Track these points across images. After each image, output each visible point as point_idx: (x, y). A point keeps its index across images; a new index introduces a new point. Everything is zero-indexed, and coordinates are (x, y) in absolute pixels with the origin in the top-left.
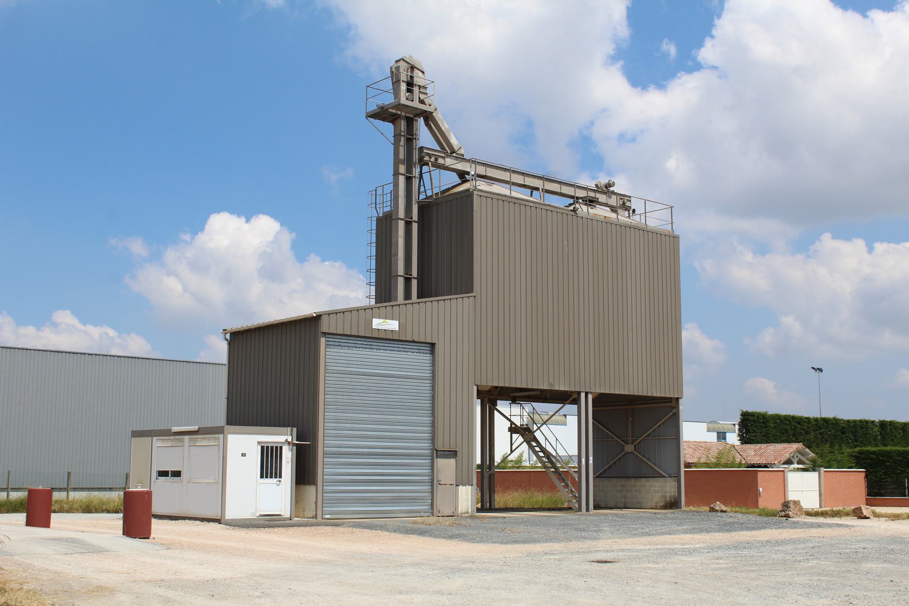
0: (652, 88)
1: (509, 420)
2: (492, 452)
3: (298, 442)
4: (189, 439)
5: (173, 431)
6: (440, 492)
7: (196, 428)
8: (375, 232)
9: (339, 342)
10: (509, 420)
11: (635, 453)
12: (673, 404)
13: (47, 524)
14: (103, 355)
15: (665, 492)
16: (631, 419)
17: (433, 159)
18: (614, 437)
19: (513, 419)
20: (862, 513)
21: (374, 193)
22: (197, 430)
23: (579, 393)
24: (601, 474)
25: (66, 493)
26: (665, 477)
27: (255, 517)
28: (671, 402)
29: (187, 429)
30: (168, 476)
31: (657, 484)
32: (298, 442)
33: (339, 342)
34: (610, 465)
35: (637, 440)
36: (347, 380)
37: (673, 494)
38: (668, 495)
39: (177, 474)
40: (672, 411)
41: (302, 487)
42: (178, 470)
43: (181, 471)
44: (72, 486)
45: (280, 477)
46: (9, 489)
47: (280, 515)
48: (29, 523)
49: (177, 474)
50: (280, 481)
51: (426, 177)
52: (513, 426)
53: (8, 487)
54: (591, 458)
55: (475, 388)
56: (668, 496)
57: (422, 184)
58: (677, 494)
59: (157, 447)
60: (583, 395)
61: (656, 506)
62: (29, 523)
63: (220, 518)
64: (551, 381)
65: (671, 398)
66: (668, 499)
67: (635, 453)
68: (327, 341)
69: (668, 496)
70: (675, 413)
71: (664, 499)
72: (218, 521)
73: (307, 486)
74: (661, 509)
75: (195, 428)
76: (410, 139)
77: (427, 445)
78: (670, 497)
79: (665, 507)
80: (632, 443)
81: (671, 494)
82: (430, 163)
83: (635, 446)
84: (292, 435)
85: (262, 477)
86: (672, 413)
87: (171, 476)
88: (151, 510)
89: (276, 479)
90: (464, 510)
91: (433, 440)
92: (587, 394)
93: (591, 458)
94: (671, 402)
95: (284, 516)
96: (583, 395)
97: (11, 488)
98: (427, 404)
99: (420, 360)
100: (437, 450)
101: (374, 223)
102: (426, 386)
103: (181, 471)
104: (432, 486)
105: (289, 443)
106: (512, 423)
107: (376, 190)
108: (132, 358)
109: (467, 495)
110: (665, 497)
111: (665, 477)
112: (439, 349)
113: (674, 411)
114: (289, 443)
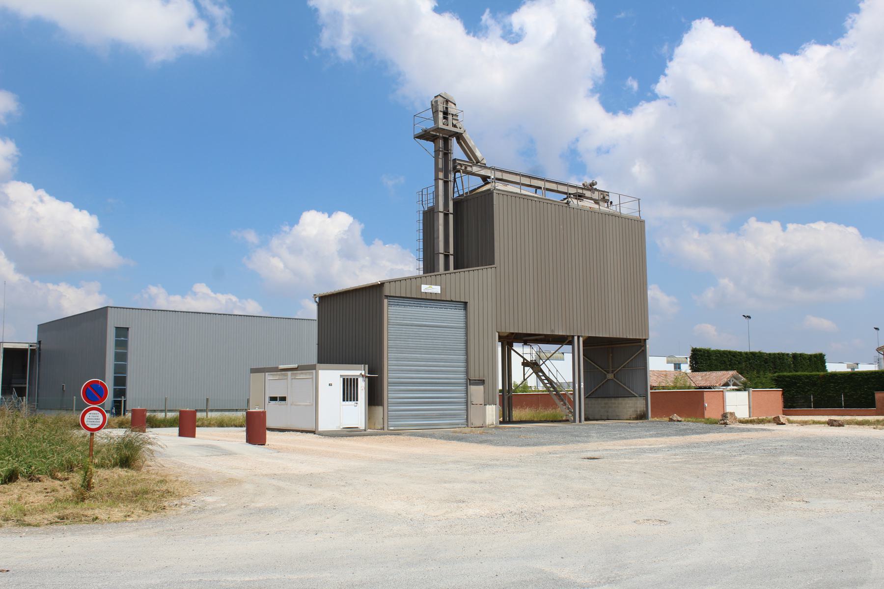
1: (522, 357)
6: (473, 410)
7: (295, 366)
10: (522, 357)
12: (642, 344)
16: (611, 355)
17: (463, 168)
18: (600, 368)
19: (525, 356)
20: (780, 421)
23: (573, 337)
24: (590, 395)
25: (164, 413)
26: (636, 397)
28: (640, 342)
34: (599, 385)
35: (615, 370)
37: (642, 409)
38: (639, 410)
39: (283, 399)
45: (357, 400)
47: (357, 428)
49: (283, 399)
51: (458, 181)
52: (525, 361)
54: (582, 384)
55: (497, 334)
56: (639, 411)
57: (456, 186)
60: (576, 338)
64: (553, 328)
65: (640, 339)
66: (639, 413)
69: (639, 411)
70: (643, 350)
72: (314, 432)
73: (377, 407)
76: (446, 154)
77: (463, 376)
78: (640, 412)
79: (637, 418)
80: (612, 373)
82: (461, 171)
83: (614, 375)
84: (364, 370)
85: (344, 400)
86: (641, 350)
91: (467, 372)
92: (579, 337)
93: (582, 384)
94: (640, 342)
96: (576, 338)
100: (470, 380)
101: (421, 215)
104: (467, 405)
105: (363, 376)
106: (524, 359)
109: (492, 411)
110: (637, 411)
111: (636, 397)
113: (643, 348)
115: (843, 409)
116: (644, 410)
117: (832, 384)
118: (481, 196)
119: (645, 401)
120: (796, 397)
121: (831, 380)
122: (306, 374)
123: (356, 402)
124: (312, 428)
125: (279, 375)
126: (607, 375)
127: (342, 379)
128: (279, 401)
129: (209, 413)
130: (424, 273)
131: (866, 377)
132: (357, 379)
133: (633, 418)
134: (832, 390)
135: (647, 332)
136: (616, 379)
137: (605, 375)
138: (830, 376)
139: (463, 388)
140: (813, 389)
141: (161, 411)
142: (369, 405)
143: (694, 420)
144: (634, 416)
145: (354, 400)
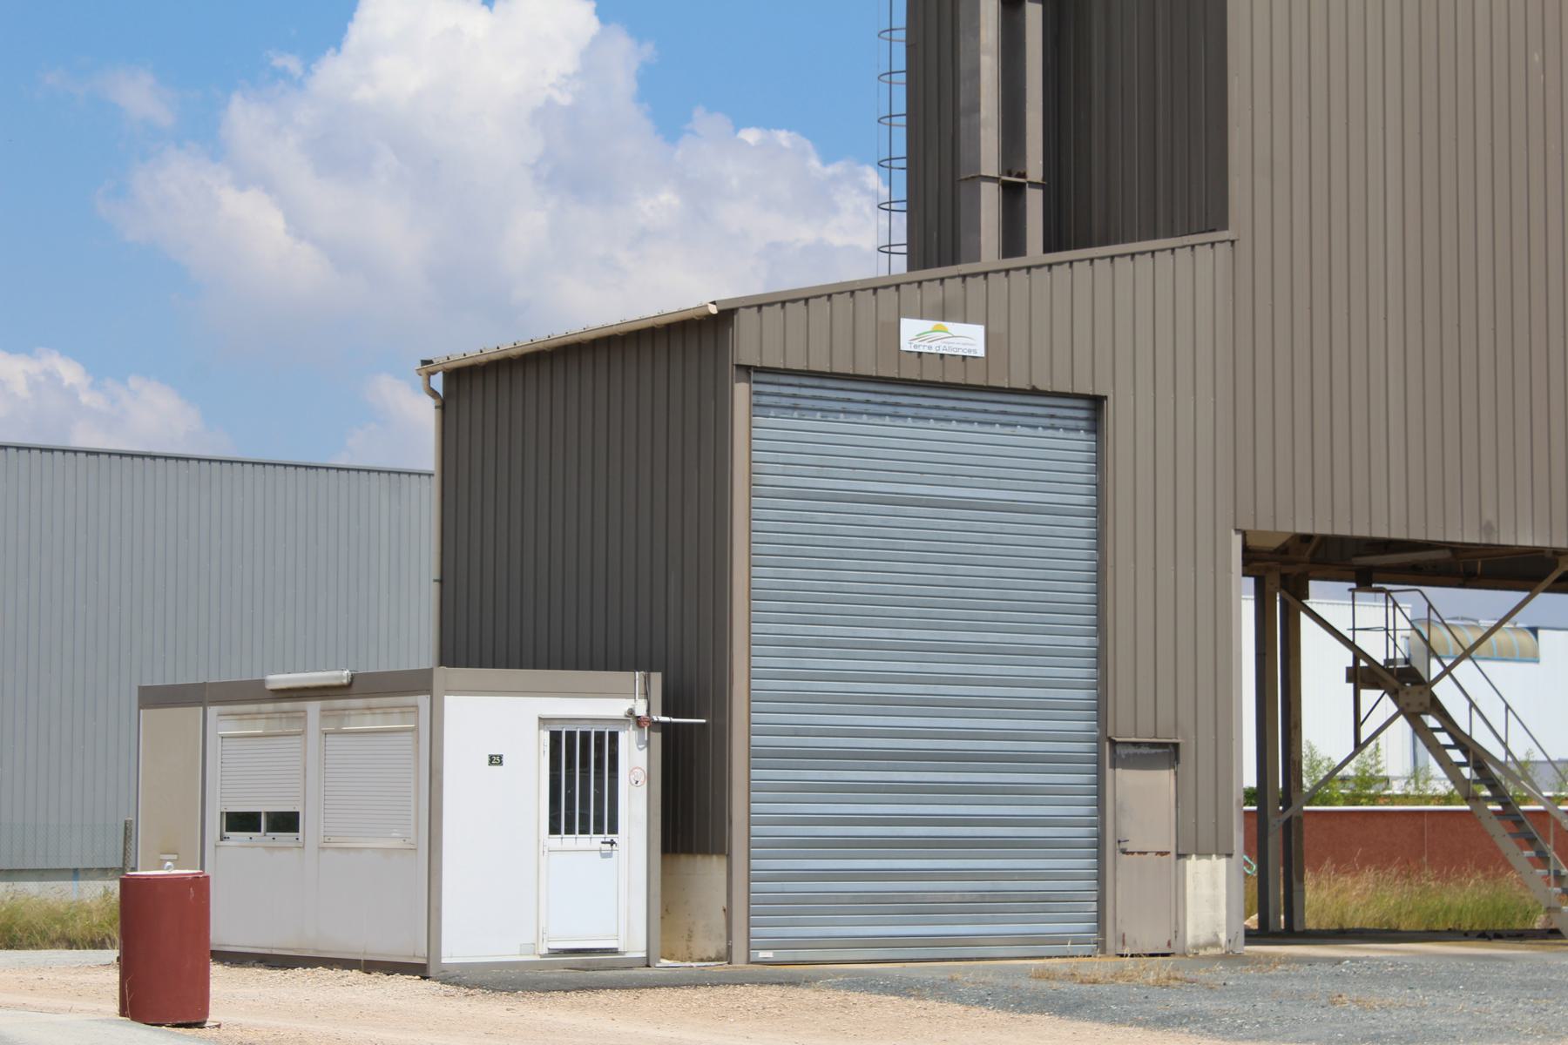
1: (1350, 644)
2: (1293, 749)
3: (666, 719)
4: (322, 710)
5: (269, 686)
6: (1125, 876)
9: (794, 396)
10: (1350, 644)
19: (1362, 641)
27: (538, 958)
30: (259, 831)
32: (666, 719)
33: (794, 396)
39: (286, 822)
43: (298, 813)
45: (614, 829)
47: (614, 951)
48: (1348, 669)
49: (286, 822)
52: (1363, 663)
55: (1237, 541)
62: (1348, 669)
63: (423, 961)
64: (1489, 515)
72: (419, 970)
73: (699, 857)
77: (1082, 725)
85: (554, 829)
89: (600, 838)
90: (1204, 936)
95: (627, 956)
98: (1082, 593)
100: (1114, 743)
103: (298, 813)
104: (1100, 857)
105: (639, 722)
106: (1358, 654)
109: (1214, 885)
112: (1118, 415)
123: (609, 837)
124: (409, 948)
125: (269, 716)
127: (546, 736)
130: (911, 266)
132: (614, 737)
139: (1085, 779)
145: (599, 831)
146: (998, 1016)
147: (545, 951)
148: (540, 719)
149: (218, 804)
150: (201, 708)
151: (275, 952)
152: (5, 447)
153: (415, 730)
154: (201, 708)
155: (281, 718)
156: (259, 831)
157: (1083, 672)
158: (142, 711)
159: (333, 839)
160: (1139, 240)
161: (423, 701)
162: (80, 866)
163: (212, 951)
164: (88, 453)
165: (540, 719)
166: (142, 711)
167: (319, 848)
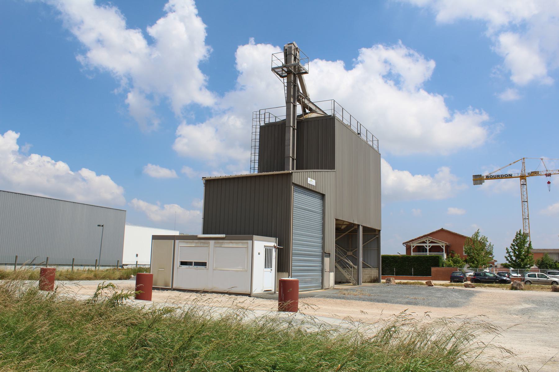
0: (14, 132)
3: (278, 247)
4: (215, 242)
5: (198, 237)
7: (177, 233)
8: (259, 133)
11: (353, 256)
12: (377, 233)
13: (149, 298)
14: (7, 192)
15: (371, 275)
20: (431, 284)
21: (258, 113)
22: (224, 237)
25: (14, 266)
26: (370, 267)
27: (263, 292)
28: (375, 232)
29: (211, 236)
30: (192, 265)
31: (366, 271)
32: (278, 247)
35: (354, 249)
36: (298, 211)
37: (375, 276)
38: (373, 276)
39: (204, 264)
40: (375, 236)
41: (280, 273)
42: (432, 274)
43: (206, 263)
44: (17, 263)
46: (16, 264)
47: (271, 290)
49: (204, 264)
50: (271, 270)
53: (15, 263)
54: (362, 258)
56: (373, 277)
58: (378, 276)
59: (180, 246)
61: (366, 281)
63: (250, 293)
66: (373, 278)
67: (353, 256)
68: (294, 189)
69: (373, 277)
71: (370, 278)
72: (249, 295)
74: (368, 283)
75: (224, 236)
77: (320, 250)
78: (374, 277)
79: (371, 282)
80: (351, 251)
81: (374, 276)
84: (276, 243)
85: (265, 268)
87: (194, 265)
88: (136, 282)
91: (323, 247)
93: (362, 258)
94: (375, 232)
97: (17, 264)
98: (320, 227)
99: (316, 202)
100: (325, 253)
101: (258, 130)
102: (319, 217)
103: (206, 263)
105: (275, 247)
107: (260, 111)
108: (22, 194)
110: (371, 277)
111: (370, 267)
112: (327, 197)
114: (275, 247)
115: (413, 276)
116: (377, 276)
117: (407, 262)
118: (322, 120)
119: (378, 271)
120: (385, 269)
121: (407, 260)
122: (236, 243)
124: (248, 291)
125: (196, 243)
126: (347, 253)
127: (265, 249)
128: (194, 265)
129: (74, 267)
130: (260, 170)
131: (427, 259)
133: (368, 281)
134: (407, 266)
135: (380, 226)
136: (354, 255)
137: (346, 252)
138: (406, 257)
139: (320, 259)
140: (395, 265)
141: (11, 264)
142: (278, 271)
143: (142, 266)
144: (369, 281)
146: (369, 303)
147: (263, 291)
148: (264, 246)
149: (179, 259)
150: (173, 240)
151: (197, 290)
152: (1, 191)
153: (247, 247)
154: (173, 240)
155: (201, 243)
156: (192, 265)
157: (320, 241)
158: (153, 240)
159: (218, 268)
160: (299, 170)
161: (250, 242)
162: (7, 263)
163: (174, 289)
164: (15, 193)
165: (264, 246)
166: (153, 240)
167: (213, 270)
